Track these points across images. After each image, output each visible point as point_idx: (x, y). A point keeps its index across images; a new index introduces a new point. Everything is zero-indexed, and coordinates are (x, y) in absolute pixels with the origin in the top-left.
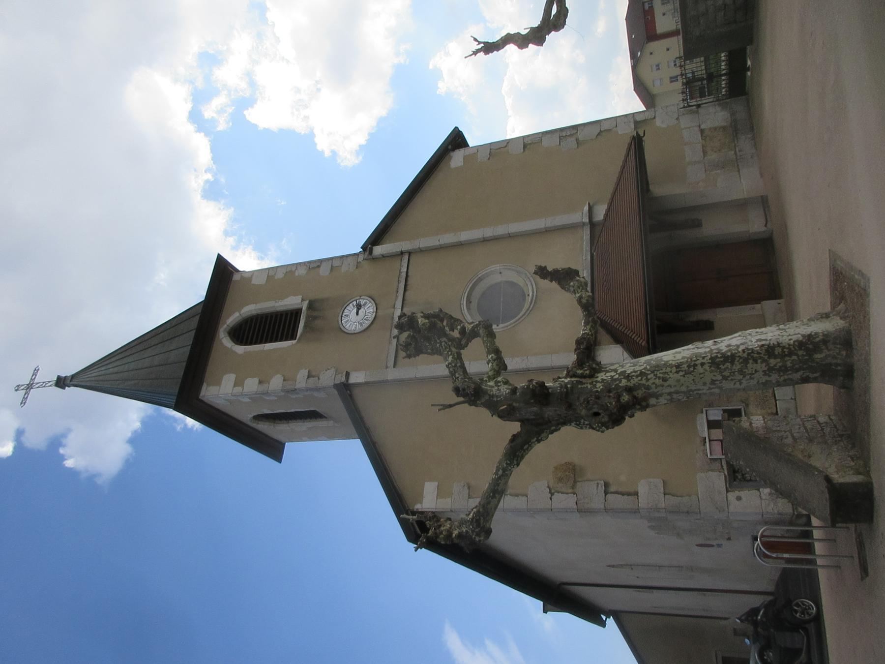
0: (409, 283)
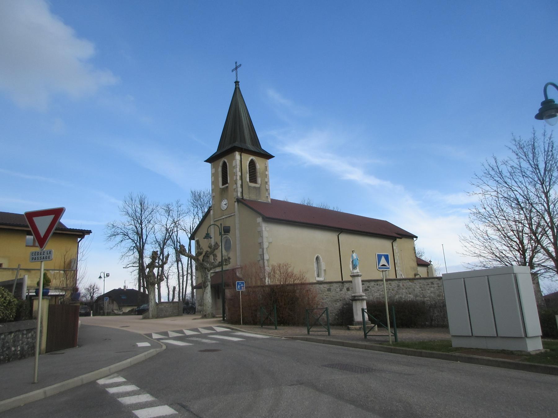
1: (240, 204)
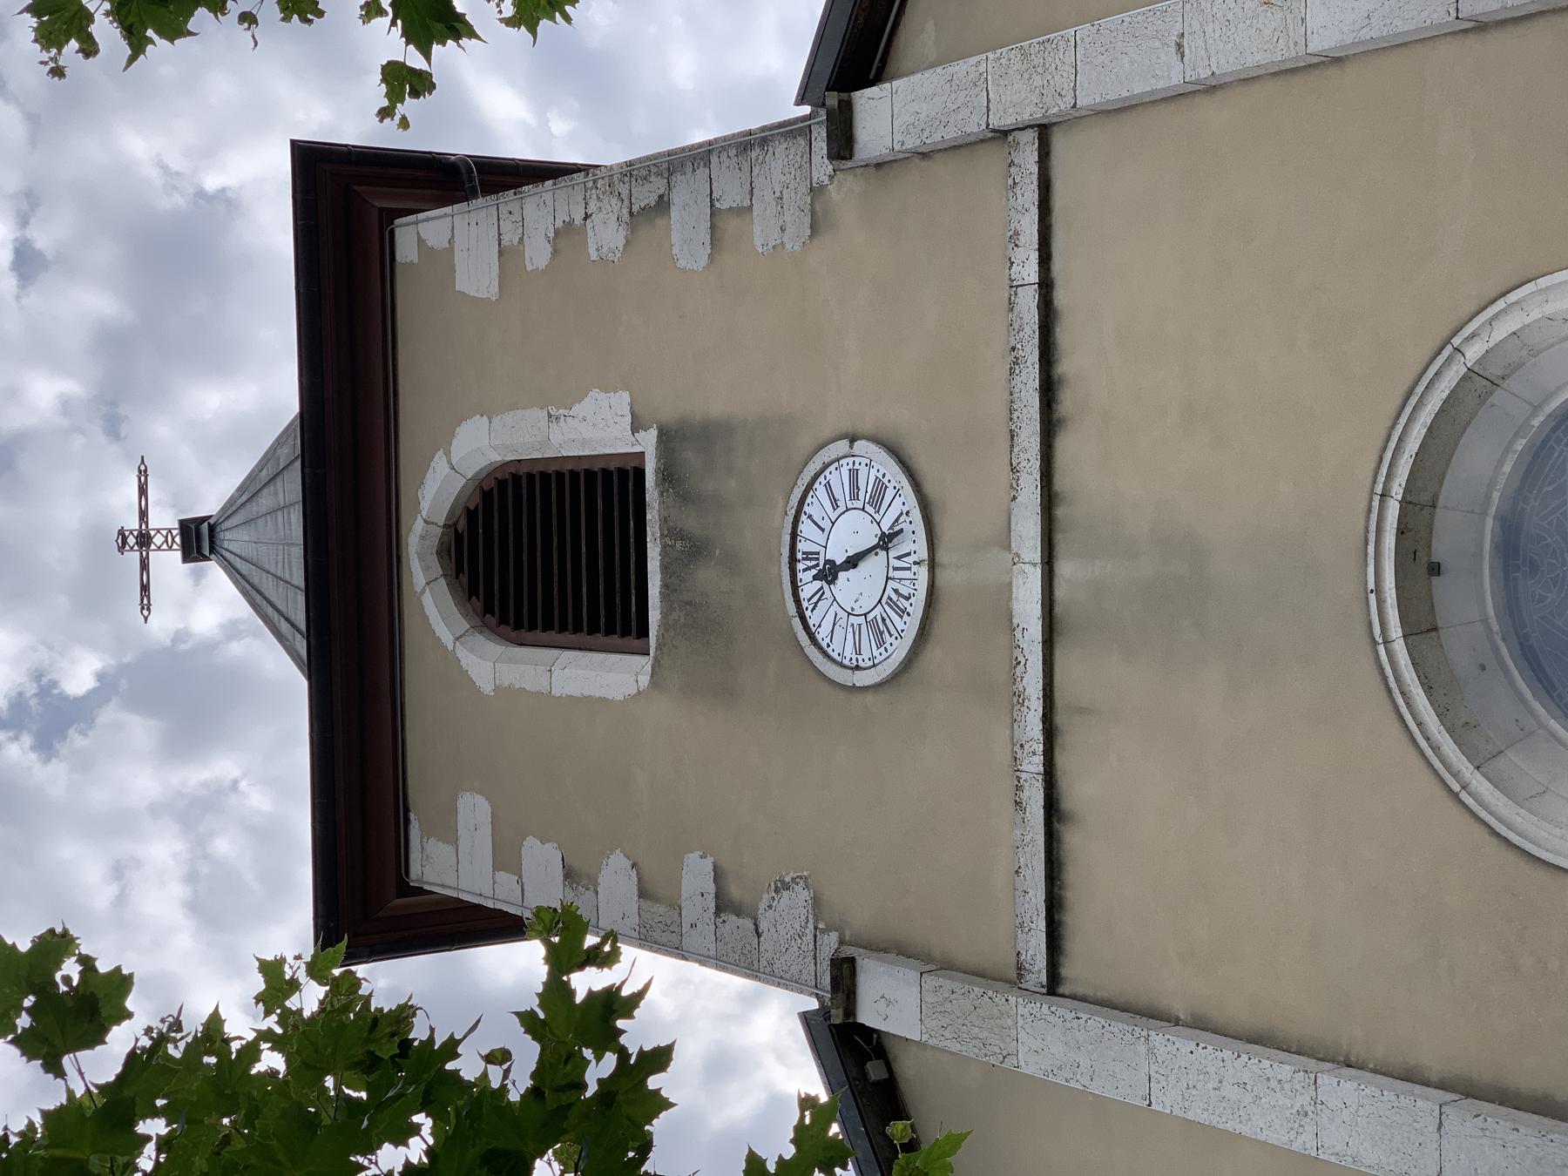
0: (1066, 367)
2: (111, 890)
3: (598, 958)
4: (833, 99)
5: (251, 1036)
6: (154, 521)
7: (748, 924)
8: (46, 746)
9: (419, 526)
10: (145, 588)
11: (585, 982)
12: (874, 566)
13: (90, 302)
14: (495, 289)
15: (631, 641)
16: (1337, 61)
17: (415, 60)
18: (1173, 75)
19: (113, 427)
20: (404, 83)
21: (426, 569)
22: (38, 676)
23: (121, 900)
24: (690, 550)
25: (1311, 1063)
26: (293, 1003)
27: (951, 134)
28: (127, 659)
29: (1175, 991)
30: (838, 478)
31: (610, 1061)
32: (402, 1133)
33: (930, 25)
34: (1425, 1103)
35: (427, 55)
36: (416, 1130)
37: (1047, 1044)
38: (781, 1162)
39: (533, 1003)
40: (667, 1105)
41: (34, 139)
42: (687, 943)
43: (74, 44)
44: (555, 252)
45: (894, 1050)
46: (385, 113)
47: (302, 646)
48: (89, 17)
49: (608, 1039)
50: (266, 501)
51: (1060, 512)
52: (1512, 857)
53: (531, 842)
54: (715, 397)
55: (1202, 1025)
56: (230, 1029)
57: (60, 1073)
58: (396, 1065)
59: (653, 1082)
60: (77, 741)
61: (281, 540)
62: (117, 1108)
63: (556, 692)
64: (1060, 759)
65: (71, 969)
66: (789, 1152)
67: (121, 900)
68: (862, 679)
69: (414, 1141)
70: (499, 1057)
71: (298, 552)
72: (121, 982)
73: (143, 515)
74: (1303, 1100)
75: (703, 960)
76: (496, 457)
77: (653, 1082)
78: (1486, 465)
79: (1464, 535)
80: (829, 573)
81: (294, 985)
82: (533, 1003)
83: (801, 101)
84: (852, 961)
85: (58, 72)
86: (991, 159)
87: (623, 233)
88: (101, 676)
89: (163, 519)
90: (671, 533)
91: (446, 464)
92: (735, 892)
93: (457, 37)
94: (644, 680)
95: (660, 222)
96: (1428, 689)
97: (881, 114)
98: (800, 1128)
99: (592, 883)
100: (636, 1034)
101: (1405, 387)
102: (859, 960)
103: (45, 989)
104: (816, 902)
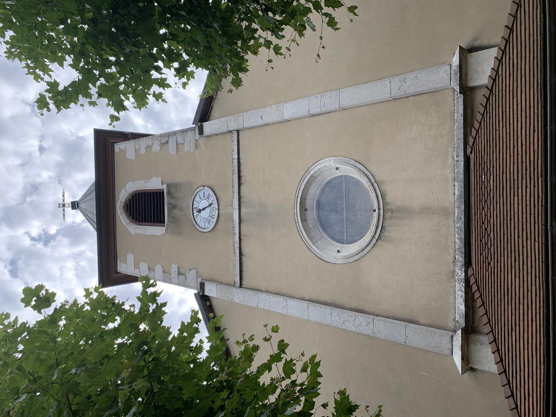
0: (242, 174)
1: (215, 112)
2: (59, 273)
3: (153, 285)
4: (199, 124)
5: (83, 303)
6: (66, 202)
7: (184, 277)
8: (46, 244)
9: (119, 202)
10: (64, 215)
11: (151, 290)
12: (208, 210)
13: (55, 157)
14: (134, 157)
15: (161, 224)
16: (289, 121)
17: (116, 114)
18: (260, 122)
19: (60, 182)
20: (114, 118)
21: (121, 211)
22: (44, 231)
23: (61, 274)
24: (173, 207)
25: (286, 298)
26: (91, 296)
27: (221, 131)
28: (63, 227)
29: (262, 287)
30: (201, 194)
31: (155, 305)
32: (114, 321)
33: (217, 111)
34: (305, 304)
35: (119, 113)
36: (116, 320)
37: (239, 296)
38: (188, 323)
39: (139, 295)
40: (166, 313)
41: (43, 126)
42: (172, 281)
43: (45, 109)
44: (146, 150)
45: (211, 299)
46: (110, 124)
47: (95, 226)
48: (49, 104)
49: (154, 301)
50: (88, 198)
51: (242, 200)
52: (320, 260)
53: (142, 263)
54: (177, 179)
55: (267, 292)
56: (78, 302)
57: (41, 313)
58: (113, 307)
59: (163, 309)
60: (52, 243)
61: (92, 205)
62: (53, 320)
63: (147, 234)
64: (242, 245)
65: (43, 292)
66: (190, 321)
67: (61, 274)
68: (205, 230)
69: (116, 322)
70: (133, 306)
71: (95, 207)
72: (54, 294)
73: (64, 200)
74: (284, 304)
75: (176, 284)
76: (135, 189)
77: (163, 309)
78: (314, 191)
79: (311, 203)
80: (199, 211)
81: (91, 293)
82: (139, 295)
83: (193, 124)
84: (204, 283)
85: (42, 115)
86: (229, 135)
87: (160, 147)
88: (57, 230)
89: (68, 200)
90: (169, 204)
91: (123, 193)
92: (181, 271)
93: (125, 110)
94: (164, 231)
95: (167, 146)
96: (305, 231)
97: (208, 127)
98: (192, 316)
99: (154, 270)
100: (160, 300)
101: (300, 178)
102: (205, 283)
103: (38, 297)
104: (197, 272)
